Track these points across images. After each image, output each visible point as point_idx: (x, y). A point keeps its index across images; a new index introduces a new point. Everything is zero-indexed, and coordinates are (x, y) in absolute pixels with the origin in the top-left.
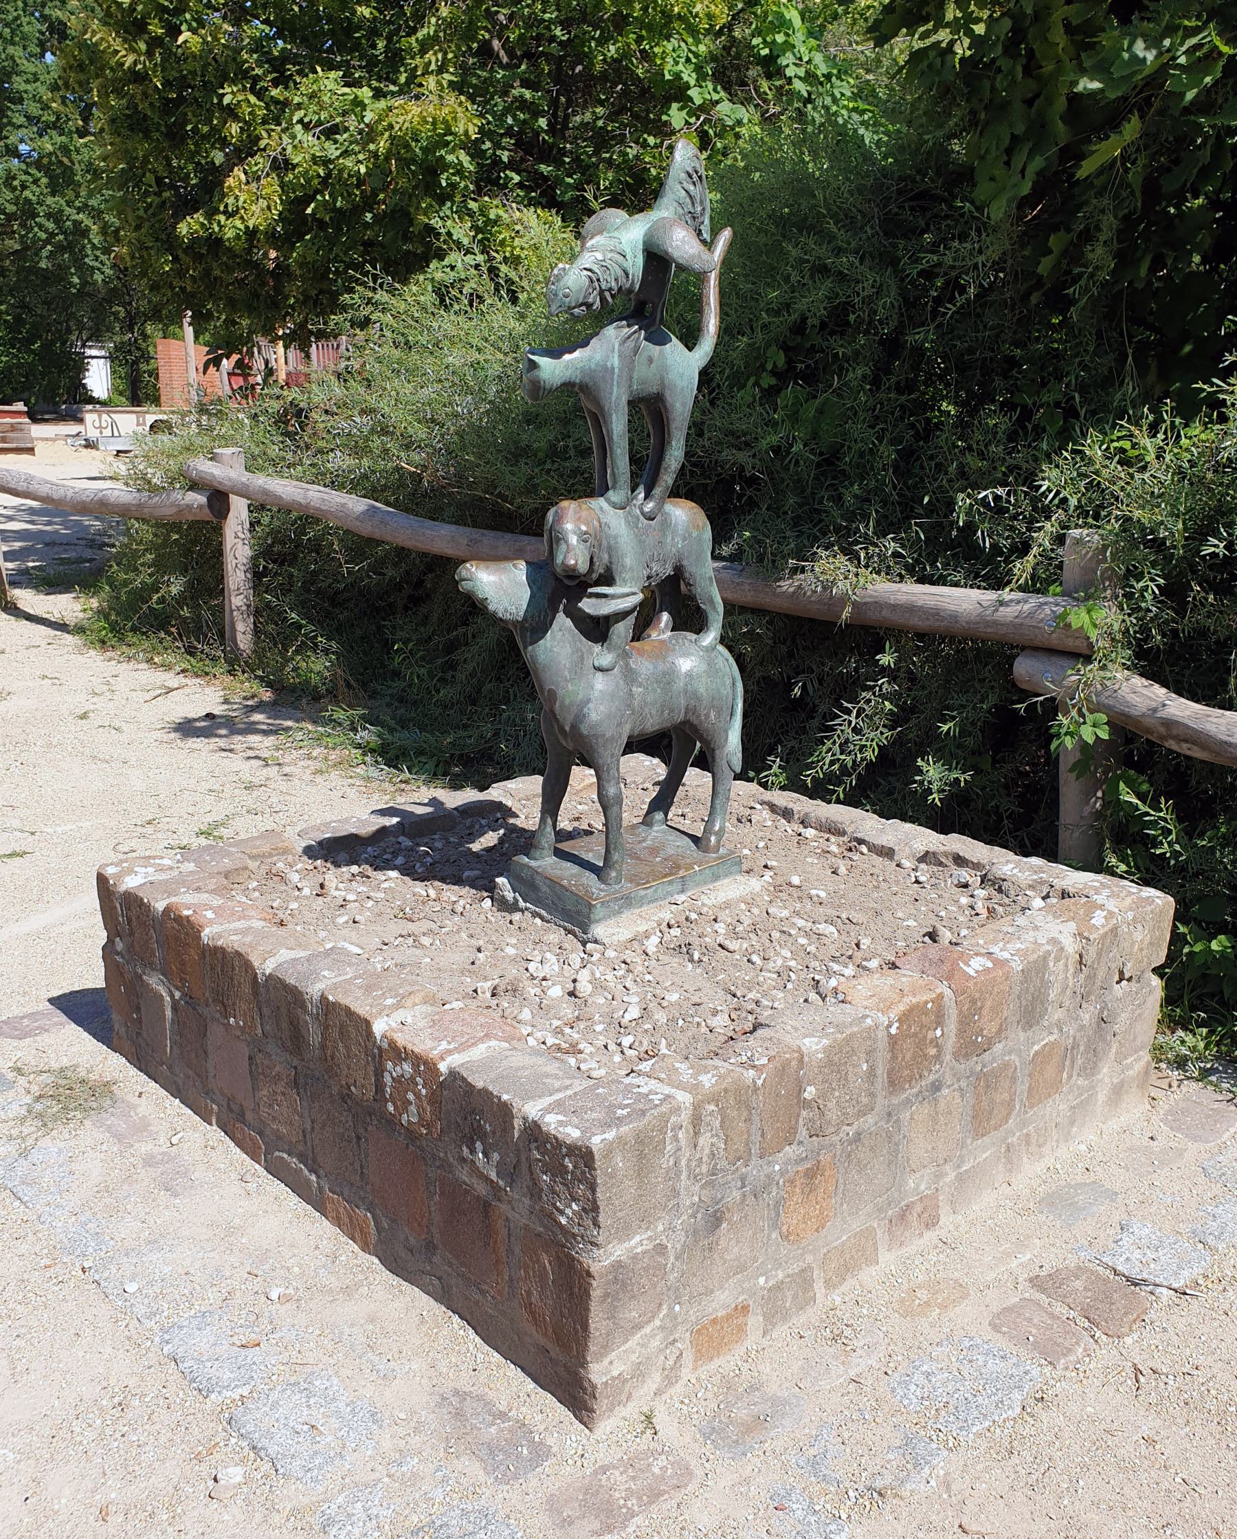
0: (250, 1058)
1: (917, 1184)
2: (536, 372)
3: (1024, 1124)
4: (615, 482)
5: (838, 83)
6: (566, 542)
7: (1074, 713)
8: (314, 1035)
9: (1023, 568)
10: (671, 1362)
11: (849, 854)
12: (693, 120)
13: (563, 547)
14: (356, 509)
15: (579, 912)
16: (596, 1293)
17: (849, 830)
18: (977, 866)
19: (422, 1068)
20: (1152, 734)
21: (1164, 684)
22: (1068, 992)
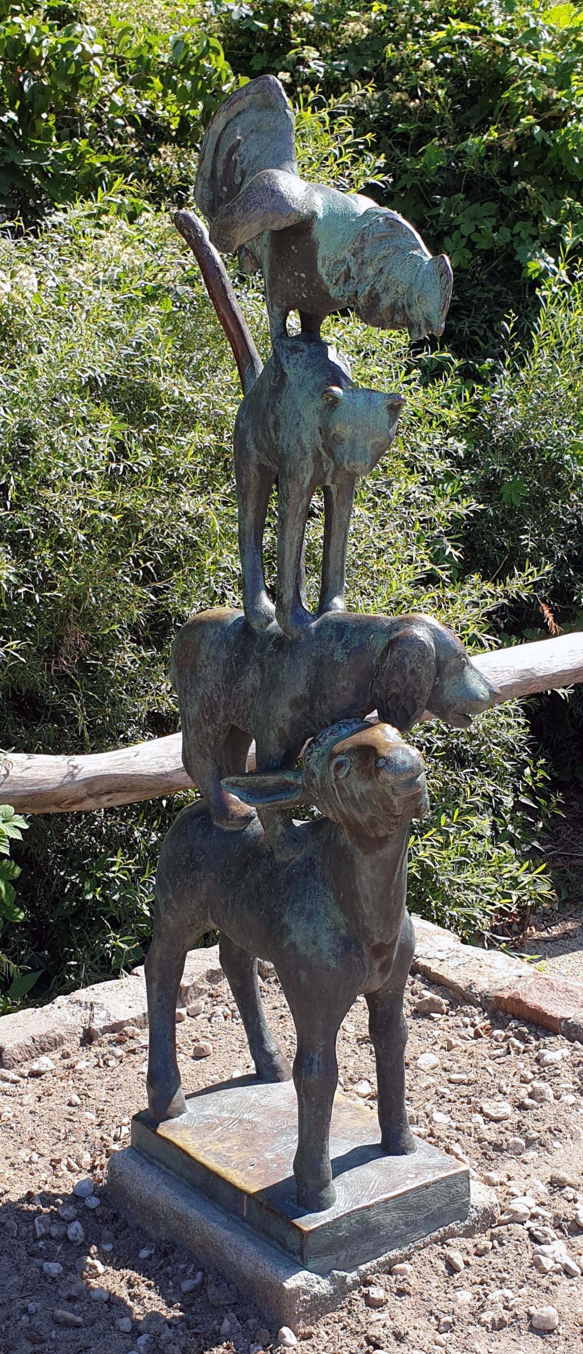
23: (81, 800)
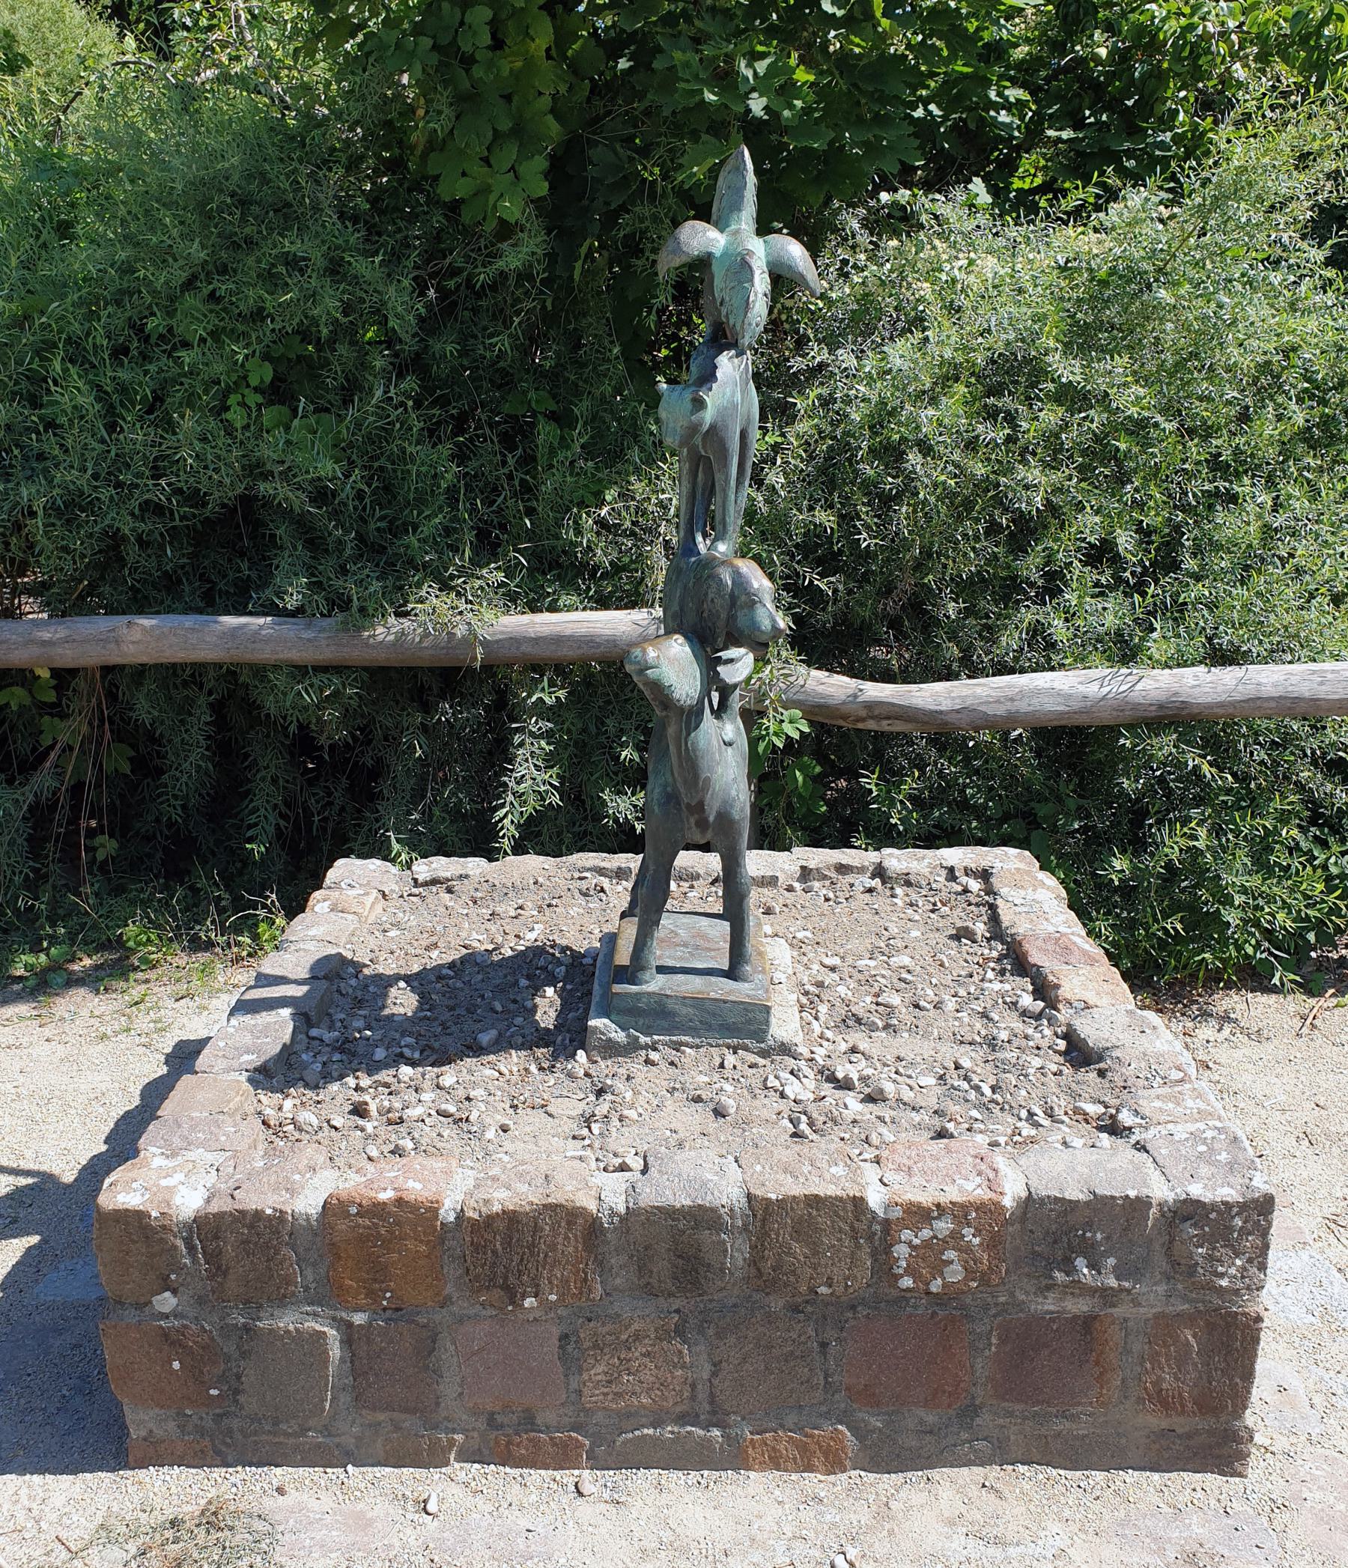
0: (564, 1338)
15: (749, 1022)
23: (863, 720)
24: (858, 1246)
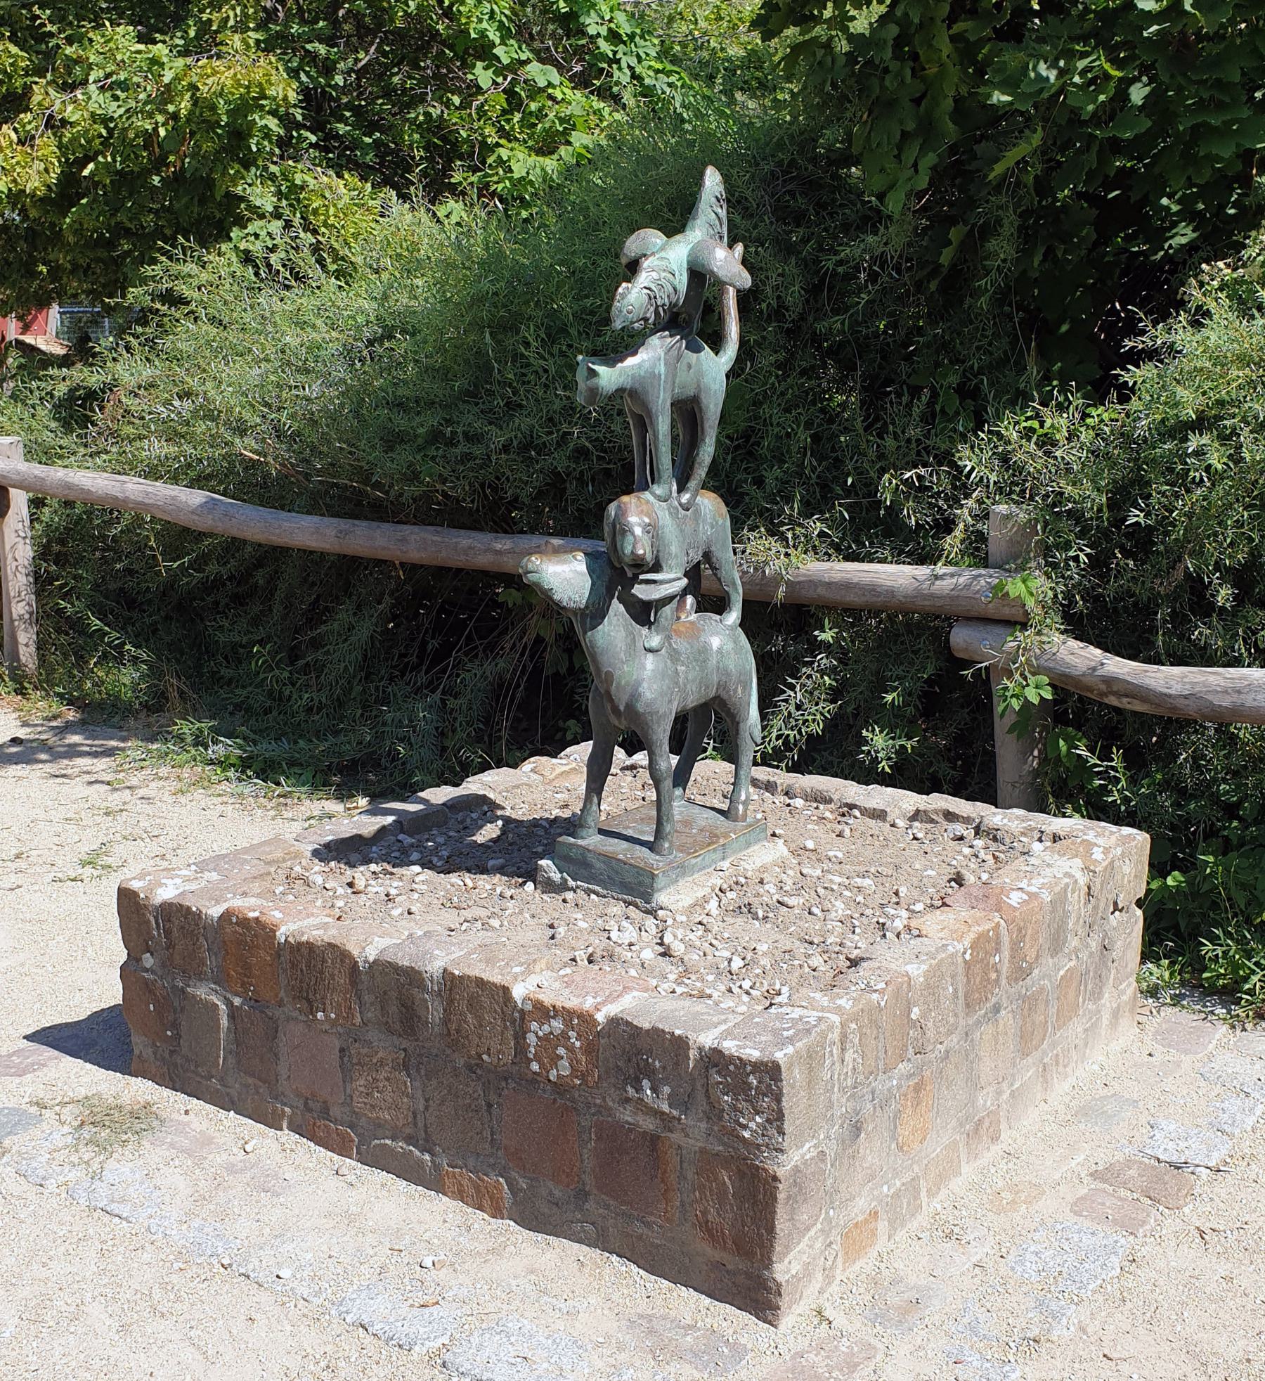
0: (342, 1050)
1: (985, 1100)
2: (595, 380)
3: (1053, 1045)
4: (660, 477)
5: (642, 43)
6: (633, 534)
7: (1017, 676)
8: (434, 1012)
9: (953, 542)
10: (830, 1263)
11: (844, 819)
12: (500, 80)
13: (630, 538)
14: (190, 502)
15: (640, 884)
16: (781, 1196)
17: (835, 797)
18: (967, 820)
19: (576, 1021)
20: (1092, 691)
21: (1098, 646)
22: (1081, 921)
24: (506, 1027)
